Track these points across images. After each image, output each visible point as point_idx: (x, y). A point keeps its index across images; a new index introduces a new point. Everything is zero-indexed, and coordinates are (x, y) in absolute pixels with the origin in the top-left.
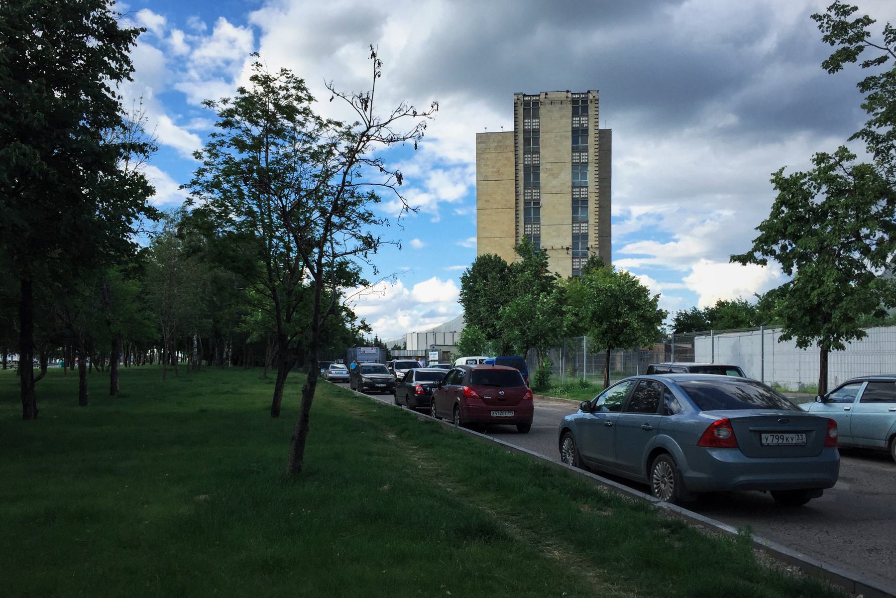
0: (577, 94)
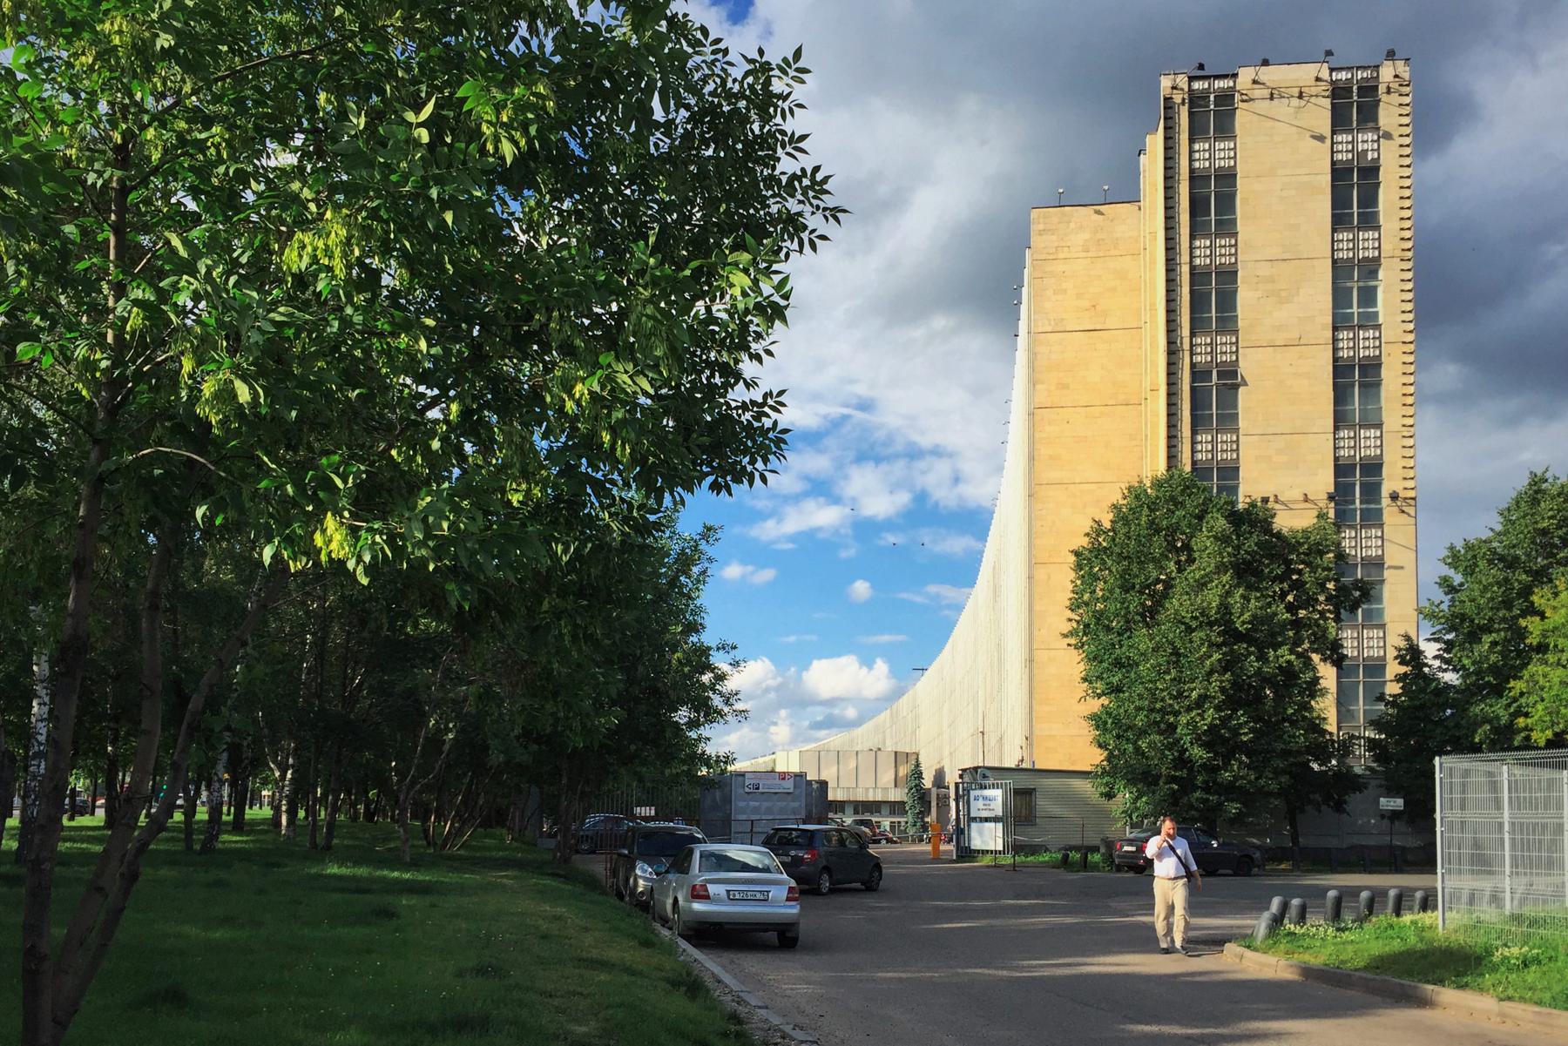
0: (1349, 69)
